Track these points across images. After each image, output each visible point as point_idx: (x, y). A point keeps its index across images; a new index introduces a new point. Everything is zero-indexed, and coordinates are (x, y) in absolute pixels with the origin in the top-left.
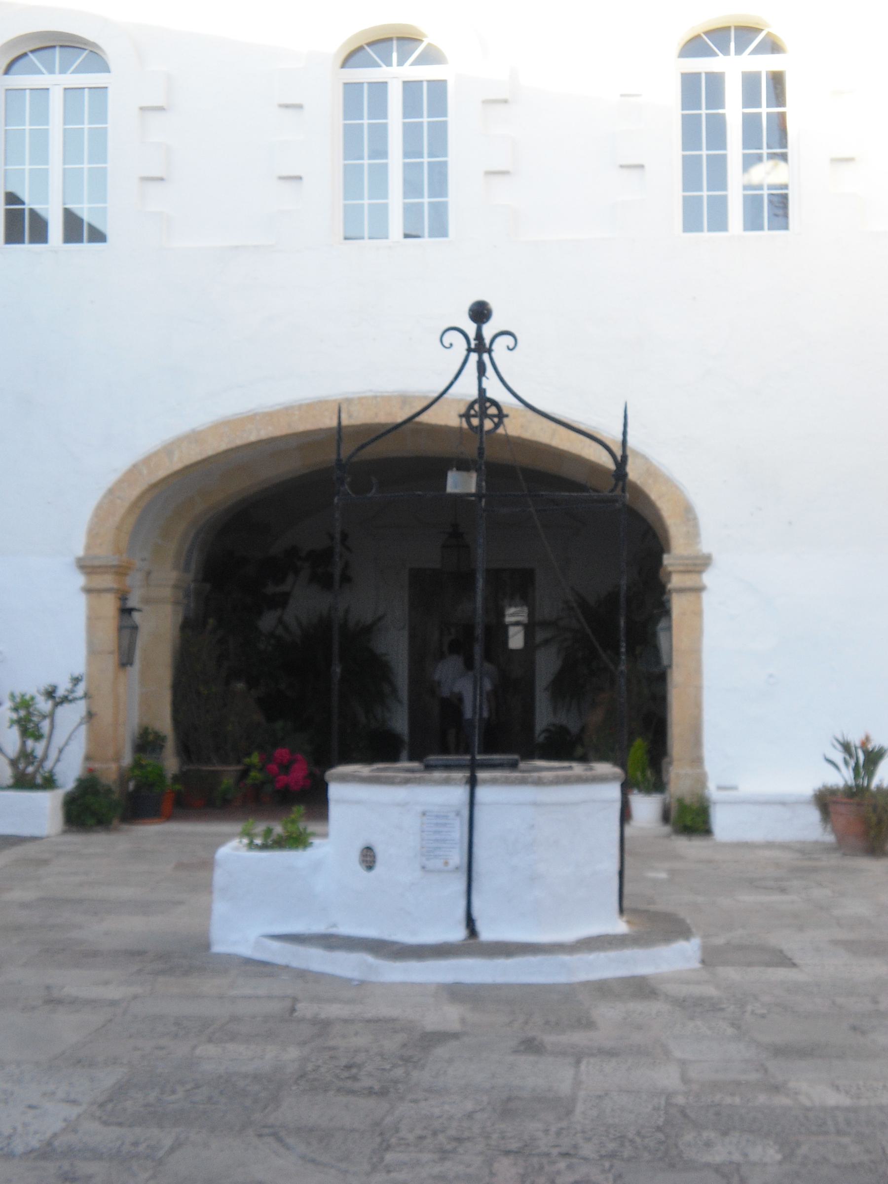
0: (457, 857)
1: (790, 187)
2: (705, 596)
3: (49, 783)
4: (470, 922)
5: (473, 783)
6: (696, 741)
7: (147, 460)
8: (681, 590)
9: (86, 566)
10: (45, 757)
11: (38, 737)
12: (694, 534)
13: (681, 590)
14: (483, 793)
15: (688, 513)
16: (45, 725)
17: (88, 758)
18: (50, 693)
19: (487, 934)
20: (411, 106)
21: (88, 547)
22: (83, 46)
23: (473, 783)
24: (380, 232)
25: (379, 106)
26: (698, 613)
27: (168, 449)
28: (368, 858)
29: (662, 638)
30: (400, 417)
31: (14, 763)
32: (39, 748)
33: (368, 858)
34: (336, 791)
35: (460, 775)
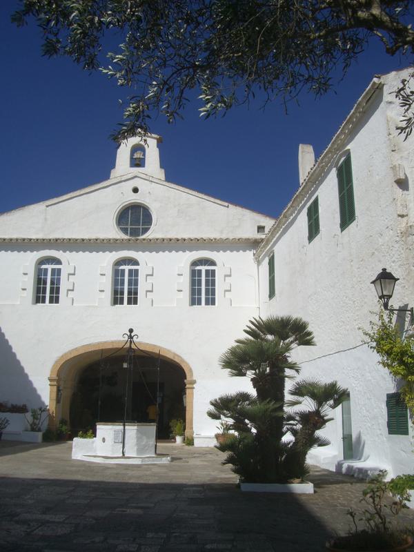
0: (121, 440)
1: (56, 305)
2: (194, 390)
3: (39, 430)
4: (123, 453)
5: (124, 425)
6: (192, 424)
7: (66, 354)
8: (189, 388)
9: (50, 380)
10: (39, 424)
11: (37, 419)
12: (192, 375)
13: (189, 388)
14: (126, 427)
15: (191, 370)
16: (39, 416)
17: (49, 425)
18: (40, 409)
19: (126, 455)
20: (130, 274)
21: (51, 375)
22: (370, 101)
23: (124, 425)
24: (199, 303)
25: (123, 275)
26: (193, 394)
27: (70, 352)
28: (104, 440)
29: (184, 399)
30: (121, 347)
31: (31, 425)
32: (37, 422)
33: (104, 440)
34: (98, 427)
35: (122, 424)
